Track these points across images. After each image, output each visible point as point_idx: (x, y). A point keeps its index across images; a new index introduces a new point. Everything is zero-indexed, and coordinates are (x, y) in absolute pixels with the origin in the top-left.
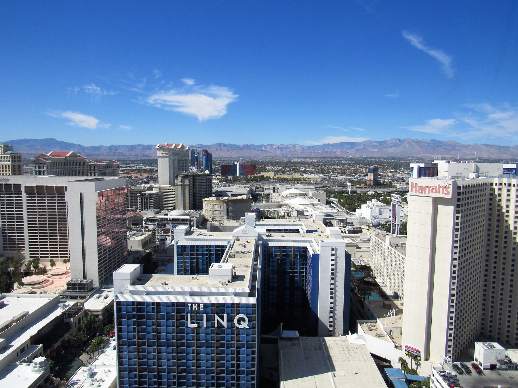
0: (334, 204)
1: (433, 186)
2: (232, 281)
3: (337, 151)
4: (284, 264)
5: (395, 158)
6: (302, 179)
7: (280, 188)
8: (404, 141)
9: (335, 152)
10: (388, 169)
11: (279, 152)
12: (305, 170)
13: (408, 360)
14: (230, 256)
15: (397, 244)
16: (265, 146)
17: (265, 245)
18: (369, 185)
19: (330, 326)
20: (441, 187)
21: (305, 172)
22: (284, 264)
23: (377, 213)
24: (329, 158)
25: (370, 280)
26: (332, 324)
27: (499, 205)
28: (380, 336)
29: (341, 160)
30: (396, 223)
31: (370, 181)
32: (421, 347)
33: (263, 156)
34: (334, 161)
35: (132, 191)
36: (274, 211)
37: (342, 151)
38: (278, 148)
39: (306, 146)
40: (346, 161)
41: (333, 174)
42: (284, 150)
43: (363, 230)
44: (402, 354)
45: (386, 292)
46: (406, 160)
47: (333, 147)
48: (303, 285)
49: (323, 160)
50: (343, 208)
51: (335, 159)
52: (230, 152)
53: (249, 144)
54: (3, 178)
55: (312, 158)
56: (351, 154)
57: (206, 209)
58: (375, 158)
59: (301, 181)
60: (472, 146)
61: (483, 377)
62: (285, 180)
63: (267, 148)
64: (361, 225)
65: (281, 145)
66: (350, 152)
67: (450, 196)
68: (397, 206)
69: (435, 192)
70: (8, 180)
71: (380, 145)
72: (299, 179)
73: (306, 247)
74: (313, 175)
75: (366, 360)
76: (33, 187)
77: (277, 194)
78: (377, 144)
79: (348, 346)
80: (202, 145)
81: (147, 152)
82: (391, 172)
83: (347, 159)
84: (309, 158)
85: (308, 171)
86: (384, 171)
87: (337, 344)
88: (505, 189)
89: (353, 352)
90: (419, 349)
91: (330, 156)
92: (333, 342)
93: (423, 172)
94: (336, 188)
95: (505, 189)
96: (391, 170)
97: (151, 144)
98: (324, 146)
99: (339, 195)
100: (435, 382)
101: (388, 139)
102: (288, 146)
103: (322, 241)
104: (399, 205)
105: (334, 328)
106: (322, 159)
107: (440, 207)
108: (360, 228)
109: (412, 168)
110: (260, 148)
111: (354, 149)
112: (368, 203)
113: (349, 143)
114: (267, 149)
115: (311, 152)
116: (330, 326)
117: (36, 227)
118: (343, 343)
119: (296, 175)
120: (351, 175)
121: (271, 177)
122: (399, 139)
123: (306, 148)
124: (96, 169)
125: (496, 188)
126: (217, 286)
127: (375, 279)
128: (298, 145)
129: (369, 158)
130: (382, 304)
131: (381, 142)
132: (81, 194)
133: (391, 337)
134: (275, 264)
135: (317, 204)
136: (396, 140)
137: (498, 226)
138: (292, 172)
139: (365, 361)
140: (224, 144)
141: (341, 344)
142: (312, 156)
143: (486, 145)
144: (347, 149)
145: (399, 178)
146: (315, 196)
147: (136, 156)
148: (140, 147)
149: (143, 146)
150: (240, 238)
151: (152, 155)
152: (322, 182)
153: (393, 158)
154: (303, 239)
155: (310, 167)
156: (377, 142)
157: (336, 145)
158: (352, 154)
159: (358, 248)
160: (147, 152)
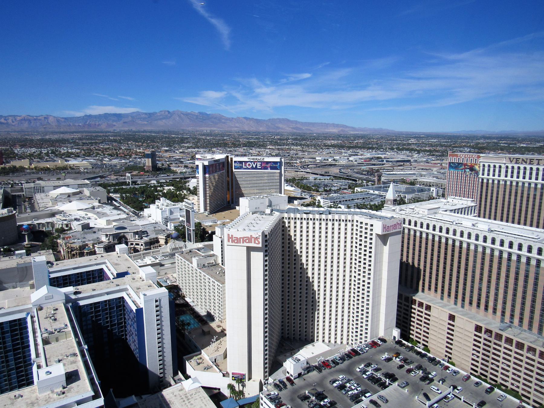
0: (116, 201)
1: (246, 237)
2: (67, 384)
4: (100, 320)
5: (166, 132)
7: (46, 186)
8: (174, 113)
9: (99, 125)
10: (162, 147)
11: (26, 125)
12: (68, 152)
13: (234, 383)
14: (46, 342)
15: (204, 265)
16: (5, 117)
17: (75, 303)
18: (148, 172)
19: (160, 373)
20: (254, 237)
21: (69, 155)
22: (100, 320)
23: (168, 213)
24: (94, 133)
25: (182, 302)
26: (162, 371)
27: (289, 235)
28: (207, 368)
29: (109, 135)
30: (191, 229)
31: (149, 166)
32: (245, 371)
34: (100, 136)
36: (48, 223)
38: (24, 119)
39: (63, 118)
40: (115, 136)
41: (104, 157)
42: (32, 123)
43: (160, 240)
44: (229, 380)
45: (199, 312)
46: (178, 135)
48: (123, 335)
49: (87, 136)
50: (128, 207)
51: (102, 134)
53: (17, 166)
55: (73, 133)
58: (146, 132)
59: (67, 169)
60: (235, 119)
61: (295, 386)
62: (46, 170)
63: (8, 119)
64: (156, 234)
67: (260, 245)
68: (191, 212)
69: (248, 242)
71: (149, 117)
73: (123, 298)
74: (80, 159)
75: (206, 404)
77: (43, 195)
78: (146, 116)
79: (186, 394)
82: (166, 151)
83: (115, 134)
84: (68, 132)
85: (72, 153)
86: (159, 150)
87: (175, 396)
88: (292, 222)
89: (192, 399)
90: (244, 373)
91: (94, 129)
92: (171, 395)
93: (207, 170)
94: (113, 178)
95: (292, 222)
96: (166, 148)
99: (118, 187)
100: (264, 404)
101: (157, 111)
102: (38, 118)
103: (145, 295)
104: (192, 211)
105: (164, 375)
106: (84, 134)
107: (252, 254)
108: (157, 238)
109: (197, 166)
112: (156, 203)
113: (115, 115)
114: (8, 121)
115: (70, 125)
116: (160, 373)
118: (181, 393)
119: (60, 162)
120: (124, 158)
121: (26, 167)
122: (168, 111)
123: (63, 120)
125: (286, 221)
126: (52, 400)
127: (186, 299)
129: (139, 132)
130: (201, 331)
131: (150, 114)
133: (217, 366)
134: (90, 322)
135: (99, 207)
136: (165, 111)
137: (289, 251)
138: (52, 156)
139: (206, 405)
141: (179, 394)
142: (73, 130)
143: (245, 118)
144: (114, 121)
145: (177, 160)
146: (93, 195)
150: (42, 306)
152: (94, 170)
153: (164, 132)
154: (117, 288)
155: (72, 146)
156: (146, 114)
157: (99, 117)
158: (119, 127)
159: (162, 265)
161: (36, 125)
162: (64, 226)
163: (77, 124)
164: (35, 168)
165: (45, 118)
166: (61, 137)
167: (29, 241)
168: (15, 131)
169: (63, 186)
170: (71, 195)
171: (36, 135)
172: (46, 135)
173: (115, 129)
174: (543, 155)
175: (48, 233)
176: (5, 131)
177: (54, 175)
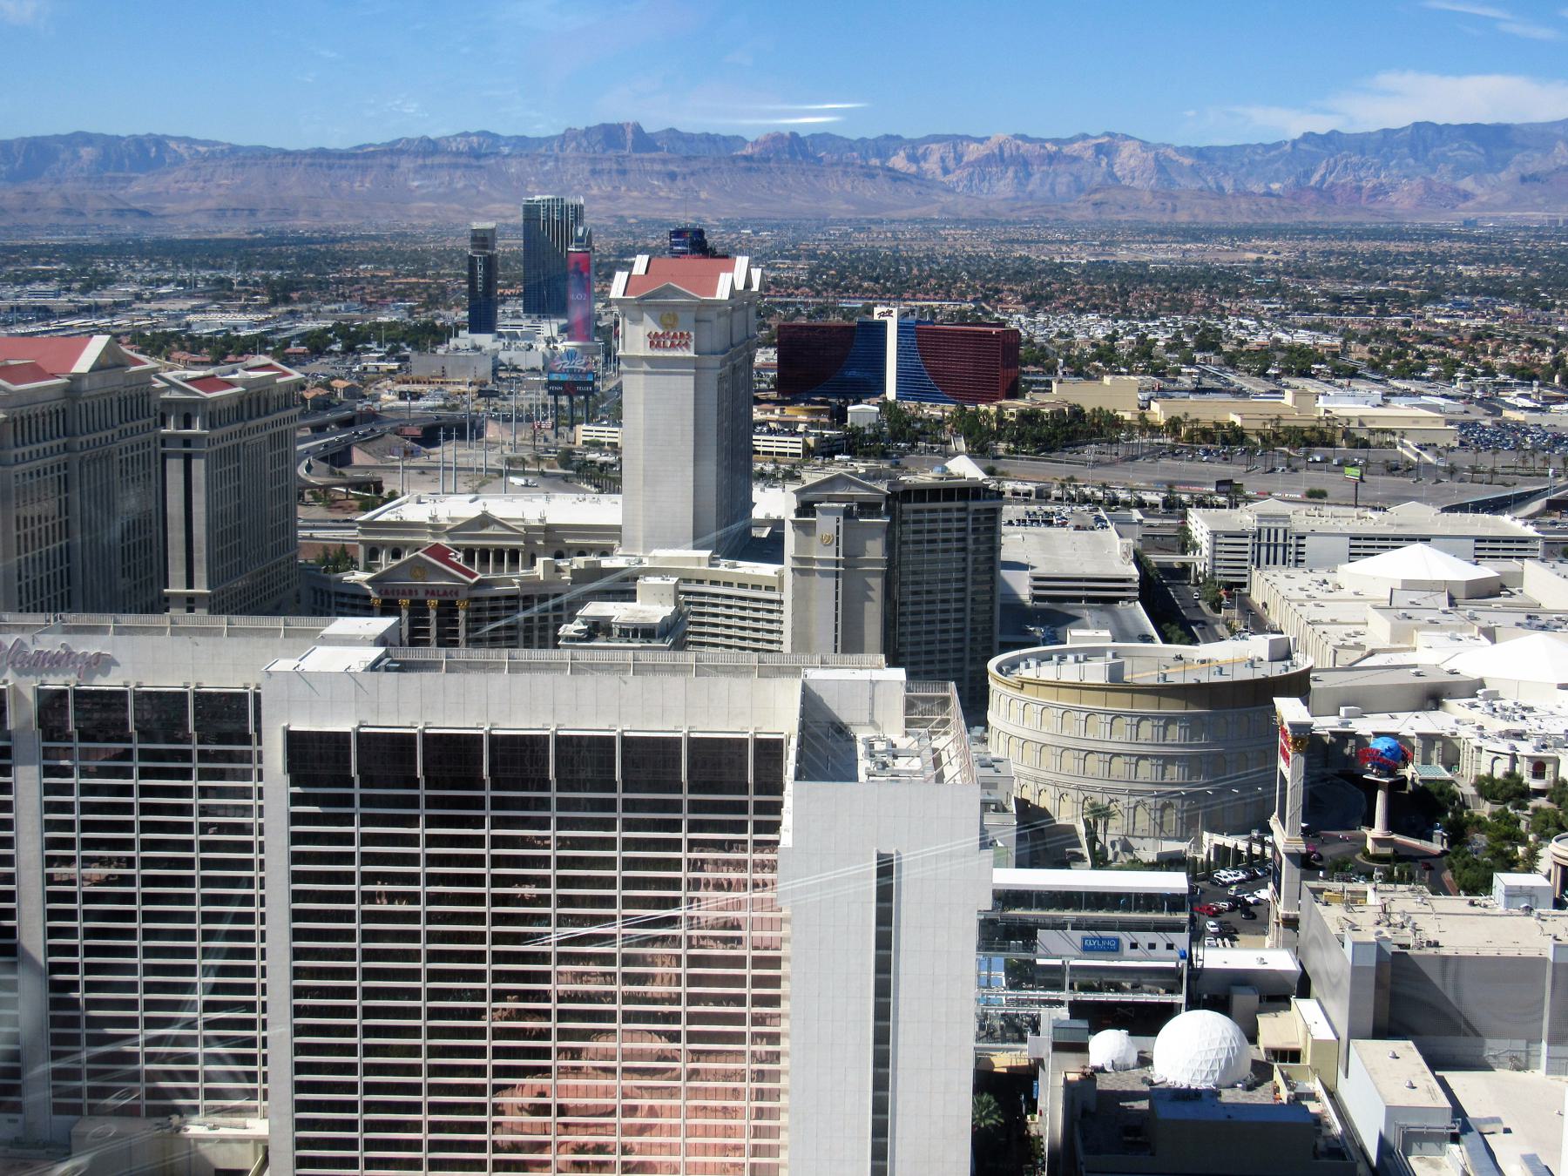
3: (1394, 188)
6: (1339, 434)
9: (1379, 191)
11: (1004, 186)
16: (914, 143)
24: (1360, 238)
33: (905, 214)
35: (477, 593)
37: (1428, 186)
38: (1000, 158)
39: (1187, 151)
40: (1486, 259)
42: (1037, 177)
47: (1363, 153)
51: (1406, 247)
52: (680, 183)
54: (69, 654)
56: (1483, 206)
57: (1026, 734)
59: (1331, 444)
63: (925, 157)
65: (1016, 137)
66: (1482, 193)
70: (102, 663)
72: (1322, 433)
76: (340, 739)
80: (496, 137)
81: (136, 188)
83: (1488, 249)
91: (1355, 218)
97: (158, 131)
98: (1303, 146)
102: (1066, 150)
110: (875, 162)
111: (1503, 175)
113: (1473, 132)
114: (925, 166)
117: (480, 1052)
121: (1128, 416)
123: (1187, 161)
124: (197, 429)
128: (1127, 138)
132: (886, 869)
140: (638, 129)
144: (1462, 169)
147: (67, 212)
148: (87, 153)
149: (108, 144)
151: (170, 207)
160: (136, 188)
161: (1053, 190)
162: (1524, 769)
163: (1258, 188)
164: (1174, 424)
165: (1100, 149)
166: (1195, 257)
167: (1391, 825)
168: (958, 222)
169: (1412, 539)
170: (1460, 594)
171: (1062, 242)
172: (1112, 243)
173: (1472, 216)
174: (5, 400)
175: (1441, 793)
176: (913, 221)
177: (1273, 470)
